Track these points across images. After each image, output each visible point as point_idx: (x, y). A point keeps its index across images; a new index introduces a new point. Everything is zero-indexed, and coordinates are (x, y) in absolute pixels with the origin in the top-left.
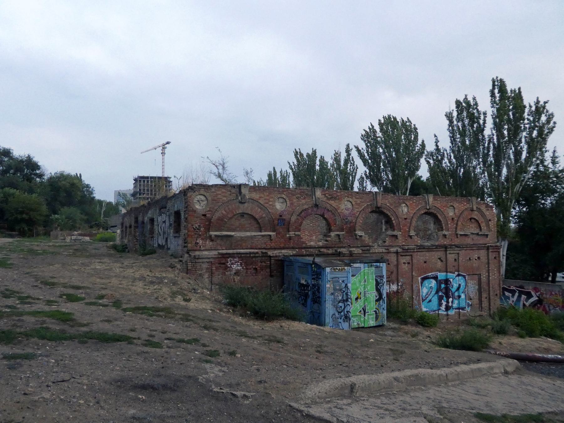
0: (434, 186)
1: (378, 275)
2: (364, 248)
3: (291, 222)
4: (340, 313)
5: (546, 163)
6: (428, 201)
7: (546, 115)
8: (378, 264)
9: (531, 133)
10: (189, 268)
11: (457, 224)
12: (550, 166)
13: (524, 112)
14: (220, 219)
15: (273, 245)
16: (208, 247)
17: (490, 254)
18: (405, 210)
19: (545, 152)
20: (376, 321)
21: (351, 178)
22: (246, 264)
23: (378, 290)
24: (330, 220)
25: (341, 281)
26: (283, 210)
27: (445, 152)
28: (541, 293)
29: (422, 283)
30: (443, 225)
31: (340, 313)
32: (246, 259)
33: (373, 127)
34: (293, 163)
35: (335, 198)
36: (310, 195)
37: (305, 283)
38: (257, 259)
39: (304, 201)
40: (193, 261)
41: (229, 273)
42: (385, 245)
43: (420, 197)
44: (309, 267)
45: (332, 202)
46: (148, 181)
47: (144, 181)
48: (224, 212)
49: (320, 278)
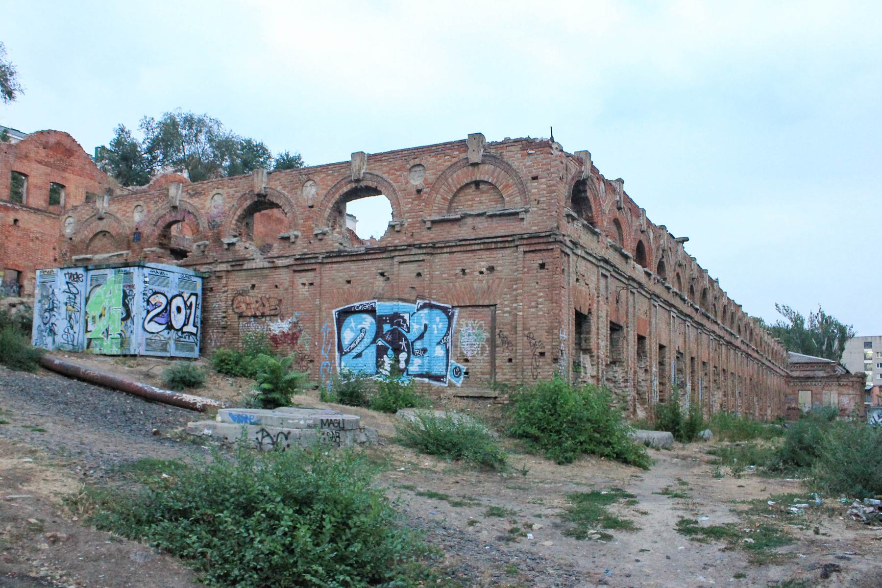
4: (45, 324)
8: (128, 269)
23: (125, 305)
31: (45, 324)
35: (200, 194)
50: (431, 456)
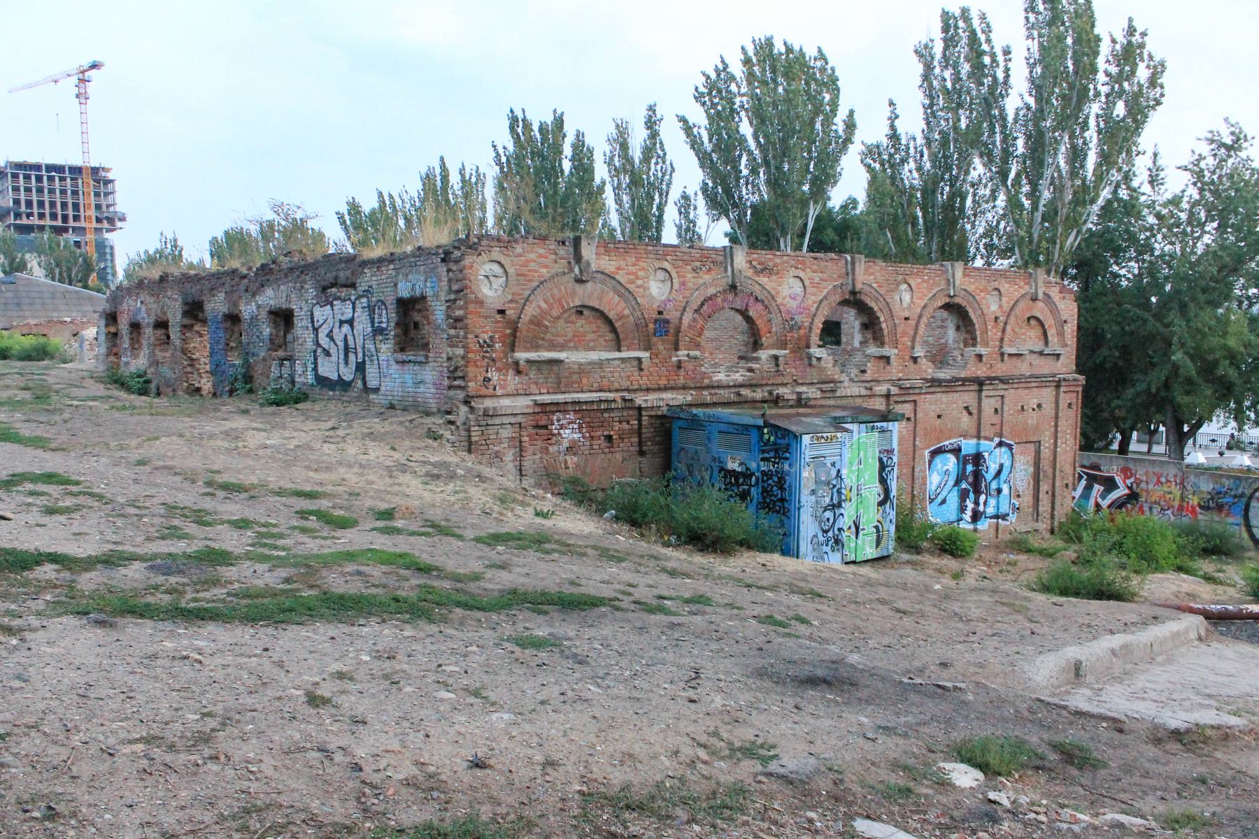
0: (881, 228)
1: (884, 448)
2: (825, 387)
3: (683, 327)
4: (826, 532)
5: (1135, 184)
6: (954, 277)
7: (1148, 67)
8: (884, 424)
9: (1110, 105)
10: (474, 439)
11: (1004, 330)
12: (1146, 188)
13: (1096, 53)
14: (536, 322)
15: (644, 382)
16: (510, 388)
17: (1062, 395)
18: (907, 297)
19: (1137, 155)
20: (877, 547)
21: (657, 197)
22: (591, 427)
23: (883, 481)
24: (759, 322)
25: (829, 465)
26: (663, 298)
27: (912, 145)
28: (1136, 479)
29: (930, 462)
30: (978, 333)
31: (826, 532)
32: (589, 414)
33: (726, 66)
34: (505, 148)
36: (721, 263)
37: (739, 469)
38: (612, 415)
39: (707, 277)
40: (482, 423)
41: (556, 448)
42: (864, 379)
43: (933, 267)
44: (754, 435)
45: (763, 280)
46: (39, 179)
47: (27, 177)
48: (544, 305)
49: (787, 459)
50: (575, 615)
